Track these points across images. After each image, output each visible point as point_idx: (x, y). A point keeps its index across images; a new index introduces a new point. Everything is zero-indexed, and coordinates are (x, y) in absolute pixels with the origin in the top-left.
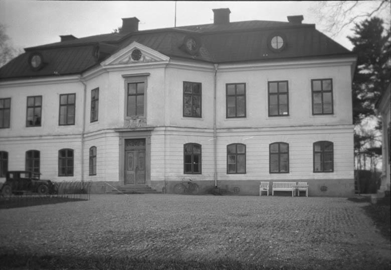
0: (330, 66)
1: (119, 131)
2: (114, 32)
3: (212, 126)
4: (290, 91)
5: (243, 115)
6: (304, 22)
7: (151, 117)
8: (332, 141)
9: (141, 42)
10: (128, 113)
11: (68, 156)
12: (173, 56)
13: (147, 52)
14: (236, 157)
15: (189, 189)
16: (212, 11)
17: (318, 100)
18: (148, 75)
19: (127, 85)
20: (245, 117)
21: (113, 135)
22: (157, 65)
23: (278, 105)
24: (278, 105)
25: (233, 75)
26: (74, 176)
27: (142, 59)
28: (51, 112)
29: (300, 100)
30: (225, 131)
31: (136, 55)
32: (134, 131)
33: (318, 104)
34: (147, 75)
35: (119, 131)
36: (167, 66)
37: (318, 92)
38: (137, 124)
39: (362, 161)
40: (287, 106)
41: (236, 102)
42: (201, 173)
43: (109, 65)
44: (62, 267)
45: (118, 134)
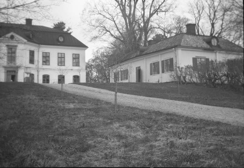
1: (5, 67)
4: (65, 57)
5: (48, 64)
7: (18, 62)
8: (34, 74)
9: (15, 32)
10: (8, 60)
13: (17, 37)
17: (75, 61)
20: (49, 65)
23: (61, 62)
24: (61, 62)
27: (14, 39)
28: (54, 60)
29: (69, 60)
30: (42, 69)
31: (12, 37)
32: (12, 67)
33: (74, 62)
34: (16, 46)
35: (5, 67)
36: (25, 43)
37: (47, 57)
38: (13, 65)
39: (233, 74)
40: (49, 61)
41: (46, 59)
44: (199, 102)
45: (4, 68)
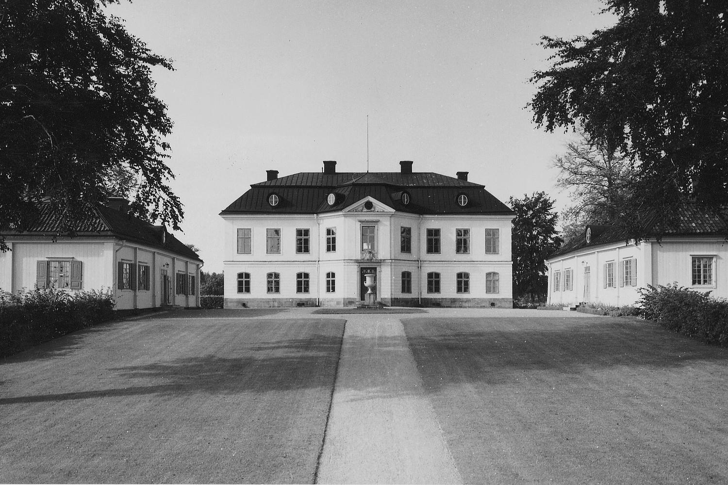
0: (713, 243)
2: (264, 178)
3: (421, 259)
6: (279, 176)
11: (435, 281)
12: (397, 210)
14: (434, 282)
15: (301, 304)
16: (484, 185)
18: (377, 222)
19: (361, 227)
21: (354, 264)
22: (383, 214)
25: (433, 222)
26: (471, 294)
27: (373, 209)
31: (369, 206)
35: (357, 261)
36: (392, 216)
42: (469, 293)
43: (348, 211)
